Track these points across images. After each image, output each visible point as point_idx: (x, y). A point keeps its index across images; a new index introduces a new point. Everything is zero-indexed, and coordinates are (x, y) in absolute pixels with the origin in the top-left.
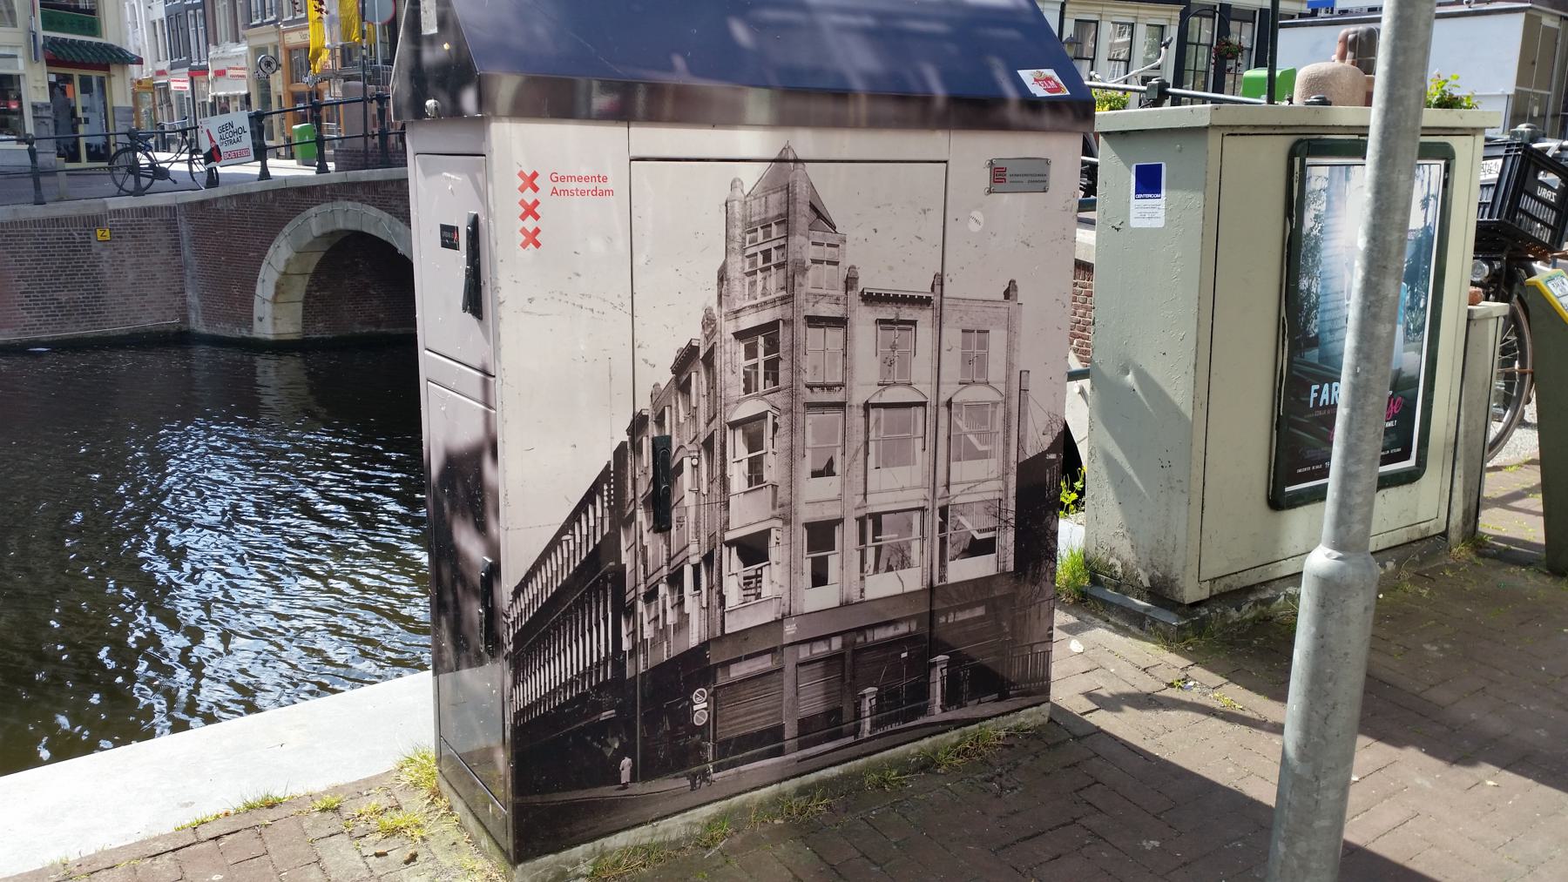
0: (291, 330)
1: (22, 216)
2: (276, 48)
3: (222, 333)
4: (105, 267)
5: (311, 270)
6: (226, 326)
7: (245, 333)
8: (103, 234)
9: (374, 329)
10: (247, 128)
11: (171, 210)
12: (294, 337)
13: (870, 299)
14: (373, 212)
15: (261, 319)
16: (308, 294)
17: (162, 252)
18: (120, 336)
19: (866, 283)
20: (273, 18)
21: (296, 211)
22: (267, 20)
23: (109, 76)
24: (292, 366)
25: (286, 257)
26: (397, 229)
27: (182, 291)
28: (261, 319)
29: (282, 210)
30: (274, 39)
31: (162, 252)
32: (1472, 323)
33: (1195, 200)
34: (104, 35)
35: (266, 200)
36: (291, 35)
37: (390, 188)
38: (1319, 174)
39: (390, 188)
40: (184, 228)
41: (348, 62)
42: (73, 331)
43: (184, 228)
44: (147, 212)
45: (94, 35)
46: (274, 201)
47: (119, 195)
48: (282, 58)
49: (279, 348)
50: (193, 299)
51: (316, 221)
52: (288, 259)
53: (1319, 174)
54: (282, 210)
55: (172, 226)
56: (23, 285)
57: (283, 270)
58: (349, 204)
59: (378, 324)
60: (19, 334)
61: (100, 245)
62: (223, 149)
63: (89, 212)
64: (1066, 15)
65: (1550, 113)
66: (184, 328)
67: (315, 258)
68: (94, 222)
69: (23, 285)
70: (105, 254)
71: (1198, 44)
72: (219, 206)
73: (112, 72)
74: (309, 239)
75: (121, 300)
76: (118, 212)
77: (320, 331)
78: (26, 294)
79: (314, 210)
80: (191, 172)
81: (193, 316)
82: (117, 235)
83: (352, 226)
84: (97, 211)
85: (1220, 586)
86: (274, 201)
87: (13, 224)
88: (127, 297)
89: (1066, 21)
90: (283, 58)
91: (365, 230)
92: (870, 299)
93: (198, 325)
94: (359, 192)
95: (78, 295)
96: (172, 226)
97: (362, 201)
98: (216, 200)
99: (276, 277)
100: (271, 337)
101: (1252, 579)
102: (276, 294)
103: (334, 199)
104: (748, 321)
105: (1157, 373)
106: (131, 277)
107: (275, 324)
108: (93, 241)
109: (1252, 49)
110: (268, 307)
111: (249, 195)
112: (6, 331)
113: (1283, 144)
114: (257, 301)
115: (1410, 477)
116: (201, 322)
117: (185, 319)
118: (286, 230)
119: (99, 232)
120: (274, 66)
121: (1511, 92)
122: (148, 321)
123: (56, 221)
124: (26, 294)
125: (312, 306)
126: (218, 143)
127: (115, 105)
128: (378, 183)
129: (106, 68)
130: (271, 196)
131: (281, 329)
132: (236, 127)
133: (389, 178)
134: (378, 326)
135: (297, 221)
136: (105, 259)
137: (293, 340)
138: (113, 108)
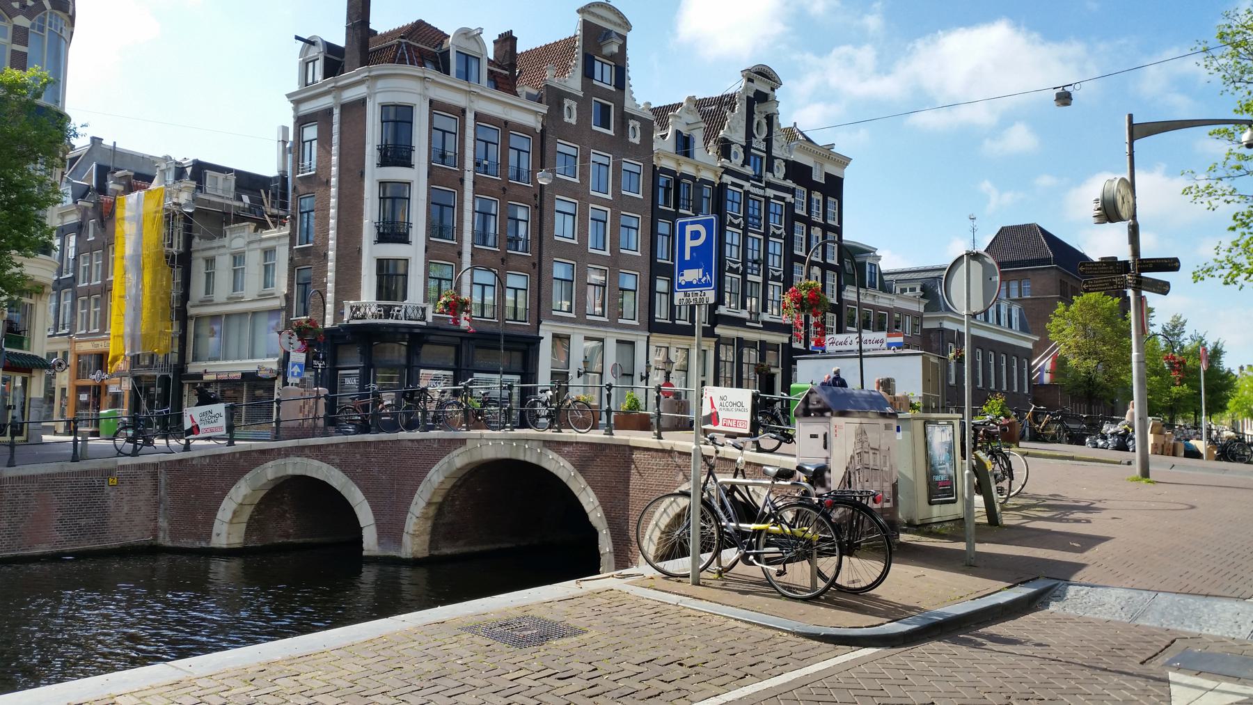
0: (238, 541)
1: (66, 470)
2: (65, 354)
3: (185, 545)
4: (111, 503)
5: (256, 501)
6: (189, 541)
7: (204, 544)
8: (113, 481)
9: (285, 540)
10: (223, 414)
11: (155, 465)
12: (238, 546)
13: (872, 449)
14: (316, 463)
15: (218, 535)
16: (251, 517)
17: (146, 493)
18: (115, 549)
19: (872, 446)
20: (66, 331)
21: (256, 464)
22: (59, 333)
23: (31, 377)
24: (236, 564)
25: (245, 493)
26: (332, 473)
27: (156, 519)
28: (218, 535)
29: (245, 464)
30: (65, 347)
31: (146, 493)
32: (1132, 215)
33: (909, 433)
34: (32, 349)
35: (234, 458)
36: (82, 344)
37: (330, 448)
38: (930, 428)
39: (330, 448)
40: (163, 478)
41: (136, 365)
42: (87, 546)
43: (163, 478)
44: (141, 467)
45: (21, 347)
46: (240, 458)
47: (118, 456)
48: (71, 360)
49: (227, 553)
50: (163, 523)
51: (270, 471)
52: (246, 495)
53: (930, 428)
54: (245, 464)
55: (154, 476)
56: (60, 515)
57: (240, 502)
58: (298, 459)
59: (288, 536)
60: (52, 548)
61: (109, 488)
62: (201, 427)
63: (106, 466)
64: (650, 343)
65: (940, 406)
66: (154, 543)
67: (262, 493)
68: (108, 473)
69: (60, 515)
70: (112, 494)
71: (725, 361)
72: (194, 462)
73: (33, 374)
74: (264, 481)
75: (118, 524)
76: (123, 467)
77: (255, 542)
78: (61, 520)
79: (270, 463)
80: (115, 445)
81: (161, 534)
82: (120, 482)
83: (298, 472)
84: (111, 466)
85: (922, 522)
86: (240, 458)
87: (60, 474)
88: (121, 522)
89: (650, 347)
90: (73, 361)
91: (309, 474)
92: (872, 449)
93: (165, 540)
94: (307, 451)
95: (91, 521)
96: (154, 476)
97: (308, 457)
98: (192, 459)
99: (234, 506)
100: (225, 546)
101: (927, 521)
102: (233, 517)
103: (287, 455)
104: (858, 451)
105: (903, 471)
106: (126, 509)
107: (228, 538)
108: (106, 485)
109: (733, 362)
110: (225, 528)
111: (219, 456)
112: (44, 546)
113: (923, 421)
114: (217, 523)
115: (954, 502)
116: (168, 539)
117: (156, 537)
118: (247, 476)
119: (111, 480)
120: (64, 366)
121: (921, 395)
122: (135, 537)
123: (86, 472)
124: (61, 520)
125: (254, 525)
126: (198, 423)
127: (32, 396)
128: (322, 445)
129: (30, 371)
130: (238, 455)
131: (232, 541)
132: (214, 413)
133: (331, 442)
134: (288, 538)
135: (258, 470)
136: (111, 497)
137: (237, 548)
138: (30, 399)
